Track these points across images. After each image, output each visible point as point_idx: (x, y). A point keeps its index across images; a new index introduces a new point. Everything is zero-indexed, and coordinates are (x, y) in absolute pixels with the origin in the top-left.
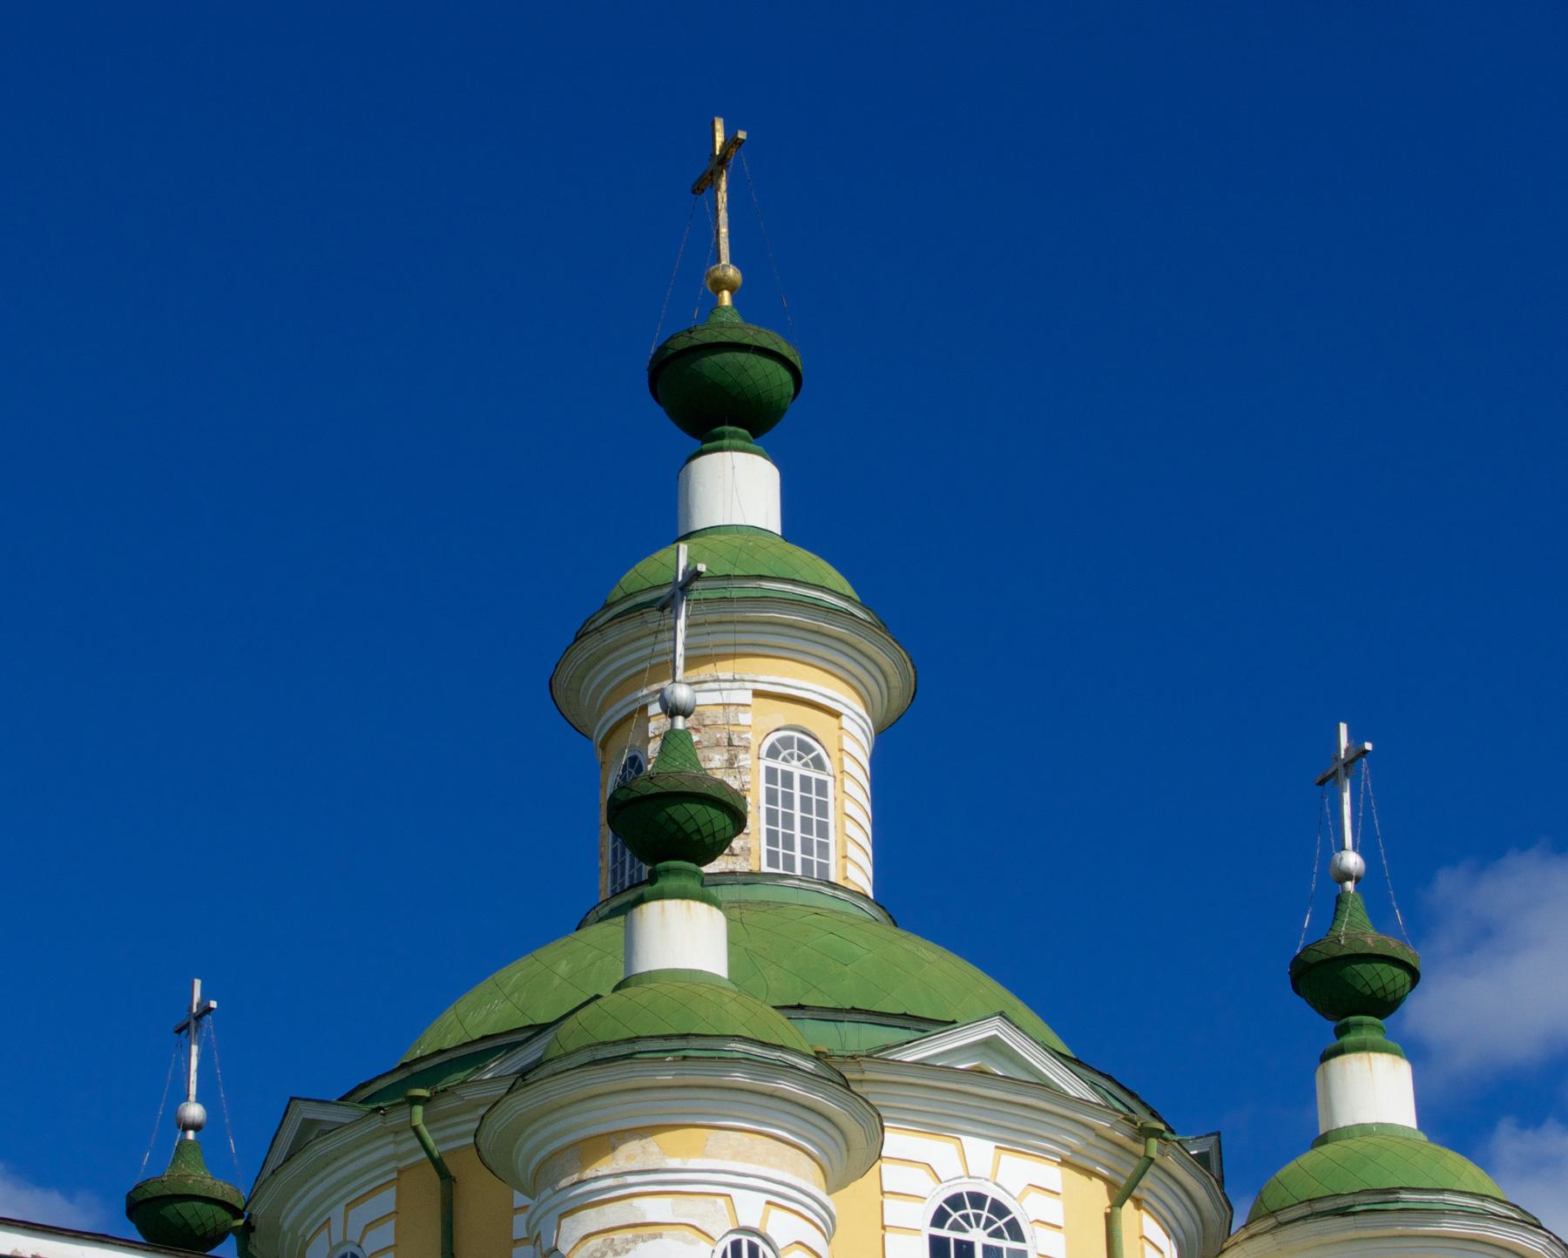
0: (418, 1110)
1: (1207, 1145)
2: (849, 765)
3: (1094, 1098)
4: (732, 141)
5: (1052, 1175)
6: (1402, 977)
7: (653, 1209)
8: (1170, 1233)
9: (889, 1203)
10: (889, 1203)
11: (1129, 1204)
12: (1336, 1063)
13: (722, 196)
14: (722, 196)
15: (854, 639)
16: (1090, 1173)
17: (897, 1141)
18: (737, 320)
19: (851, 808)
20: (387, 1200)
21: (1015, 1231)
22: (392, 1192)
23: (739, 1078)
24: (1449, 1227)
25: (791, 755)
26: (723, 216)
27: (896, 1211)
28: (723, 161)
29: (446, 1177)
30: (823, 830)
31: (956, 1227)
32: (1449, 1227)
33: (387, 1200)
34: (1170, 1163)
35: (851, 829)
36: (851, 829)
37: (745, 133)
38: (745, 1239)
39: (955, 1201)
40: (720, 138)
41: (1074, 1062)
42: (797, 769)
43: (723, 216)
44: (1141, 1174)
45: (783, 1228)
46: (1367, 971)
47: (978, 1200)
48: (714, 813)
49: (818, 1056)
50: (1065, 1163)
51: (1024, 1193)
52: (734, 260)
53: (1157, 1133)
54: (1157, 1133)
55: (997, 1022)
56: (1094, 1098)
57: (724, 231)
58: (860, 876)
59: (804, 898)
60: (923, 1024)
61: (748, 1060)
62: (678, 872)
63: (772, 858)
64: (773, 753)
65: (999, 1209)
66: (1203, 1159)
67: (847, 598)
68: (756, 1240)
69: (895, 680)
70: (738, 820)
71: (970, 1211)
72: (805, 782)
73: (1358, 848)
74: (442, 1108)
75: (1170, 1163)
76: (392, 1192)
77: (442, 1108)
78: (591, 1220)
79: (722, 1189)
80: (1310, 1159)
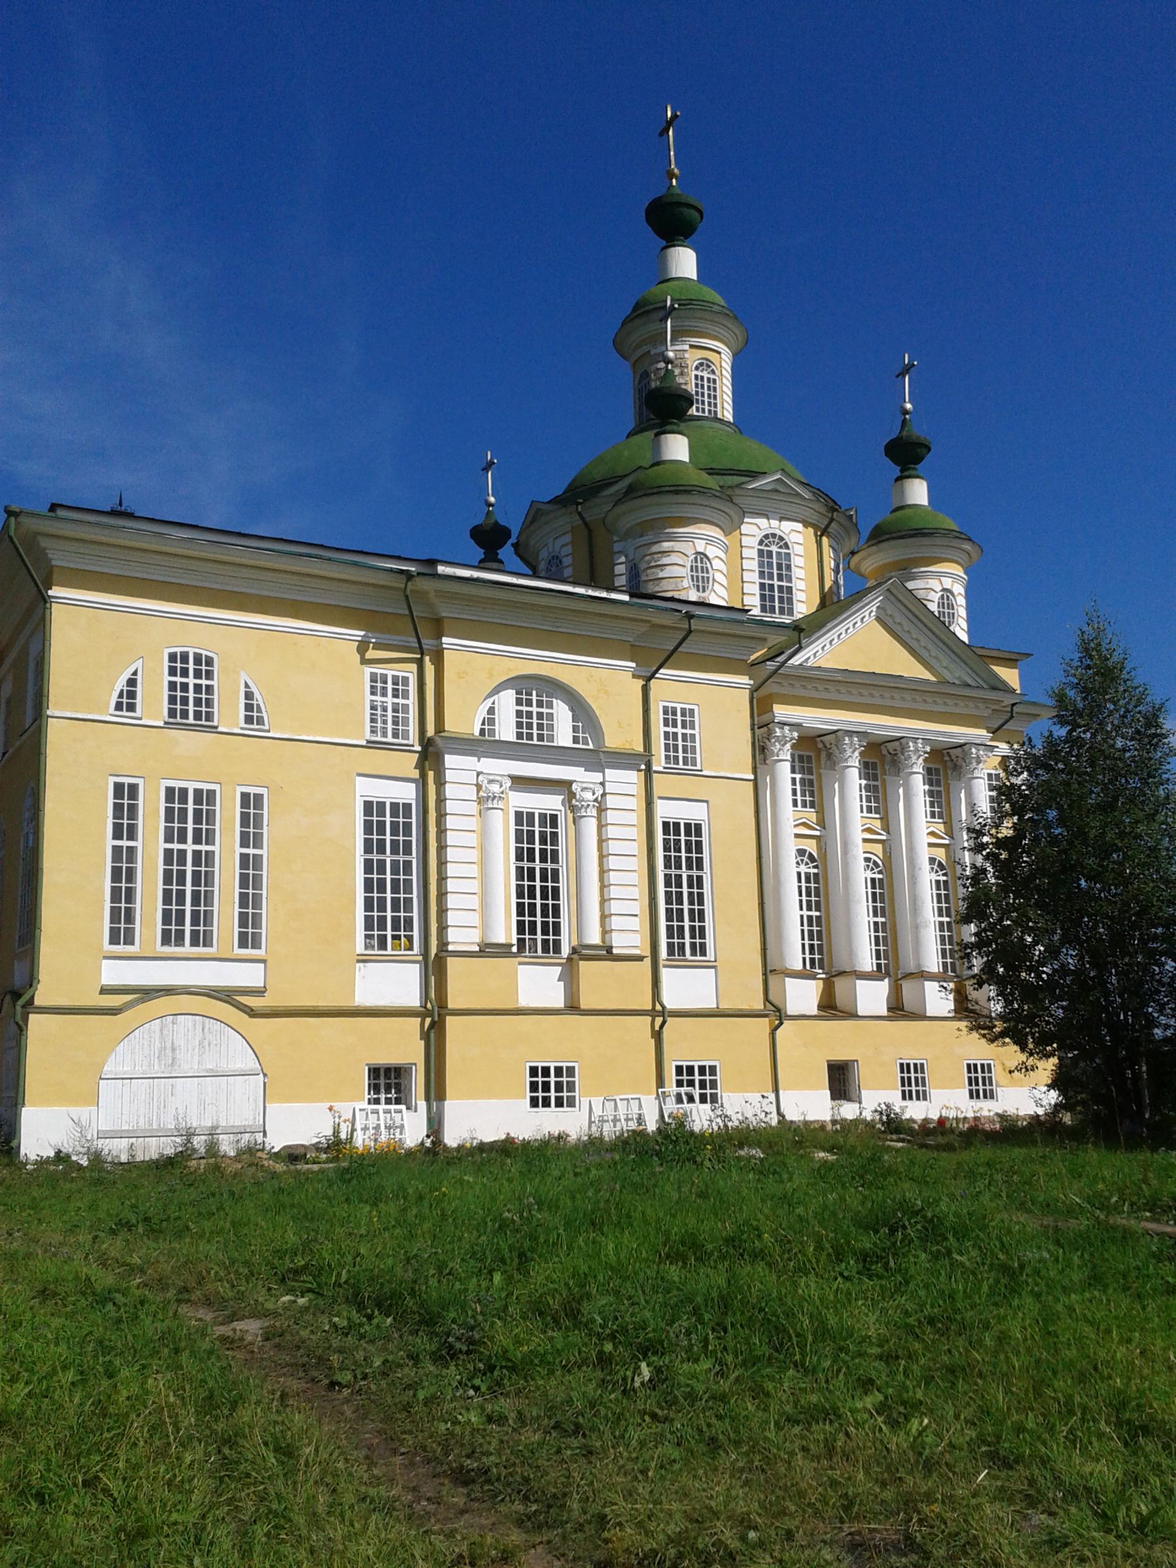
4: (674, 116)
5: (799, 526)
12: (663, 436)
20: (568, 538)
21: (786, 546)
27: (746, 541)
28: (669, 123)
29: (590, 531)
31: (766, 545)
39: (766, 536)
42: (706, 375)
45: (712, 551)
47: (774, 535)
60: (754, 475)
64: (697, 368)
65: (781, 539)
69: (740, 338)
72: (709, 379)
73: (910, 401)
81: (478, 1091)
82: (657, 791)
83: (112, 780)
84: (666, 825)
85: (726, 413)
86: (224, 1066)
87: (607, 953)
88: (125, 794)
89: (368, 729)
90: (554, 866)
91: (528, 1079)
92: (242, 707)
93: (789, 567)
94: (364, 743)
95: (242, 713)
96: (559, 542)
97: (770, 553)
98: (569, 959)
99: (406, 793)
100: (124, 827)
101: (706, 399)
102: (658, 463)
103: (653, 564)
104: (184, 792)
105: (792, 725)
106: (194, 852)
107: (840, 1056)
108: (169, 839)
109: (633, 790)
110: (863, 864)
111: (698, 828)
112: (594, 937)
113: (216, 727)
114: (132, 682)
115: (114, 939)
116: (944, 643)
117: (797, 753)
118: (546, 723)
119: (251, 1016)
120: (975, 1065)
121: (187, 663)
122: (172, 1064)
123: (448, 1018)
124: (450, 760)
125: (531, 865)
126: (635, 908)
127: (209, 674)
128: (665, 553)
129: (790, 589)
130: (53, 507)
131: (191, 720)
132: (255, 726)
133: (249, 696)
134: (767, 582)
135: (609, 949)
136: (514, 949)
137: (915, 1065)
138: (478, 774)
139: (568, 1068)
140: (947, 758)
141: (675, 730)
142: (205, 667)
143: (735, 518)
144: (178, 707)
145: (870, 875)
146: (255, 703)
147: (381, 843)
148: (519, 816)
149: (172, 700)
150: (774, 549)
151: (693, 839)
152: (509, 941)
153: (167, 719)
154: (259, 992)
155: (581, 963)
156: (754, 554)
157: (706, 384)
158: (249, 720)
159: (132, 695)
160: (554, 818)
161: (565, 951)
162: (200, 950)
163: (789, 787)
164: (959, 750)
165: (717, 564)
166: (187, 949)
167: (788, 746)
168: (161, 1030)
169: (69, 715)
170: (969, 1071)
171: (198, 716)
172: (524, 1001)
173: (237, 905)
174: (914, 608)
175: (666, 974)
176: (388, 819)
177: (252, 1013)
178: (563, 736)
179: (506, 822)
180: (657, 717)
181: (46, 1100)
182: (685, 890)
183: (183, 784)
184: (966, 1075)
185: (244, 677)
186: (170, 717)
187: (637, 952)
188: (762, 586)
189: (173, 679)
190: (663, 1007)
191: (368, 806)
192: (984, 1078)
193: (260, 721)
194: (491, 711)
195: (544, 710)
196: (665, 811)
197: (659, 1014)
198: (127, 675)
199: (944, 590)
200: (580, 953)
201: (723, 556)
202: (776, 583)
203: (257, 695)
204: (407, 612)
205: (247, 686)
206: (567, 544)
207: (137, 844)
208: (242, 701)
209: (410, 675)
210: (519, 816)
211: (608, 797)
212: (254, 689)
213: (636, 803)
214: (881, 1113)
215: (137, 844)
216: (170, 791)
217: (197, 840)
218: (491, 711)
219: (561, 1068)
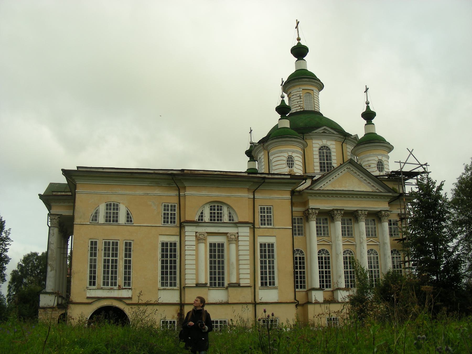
5: (334, 143)
21: (329, 149)
25: (322, 254)
31: (322, 150)
39: (322, 147)
47: (325, 146)
51: (330, 145)
65: (327, 147)
68: (291, 156)
71: (324, 148)
74: (390, 194)
77: (390, 194)
84: (261, 245)
88: (94, 244)
99: (175, 239)
108: (105, 256)
116: (137, 181)
118: (220, 216)
138: (196, 233)
147: (265, 256)
148: (211, 245)
154: (130, 298)
156: (317, 153)
171: (218, 220)
176: (217, 248)
178: (226, 218)
179: (206, 247)
180: (258, 209)
188: (320, 163)
191: (163, 244)
193: (131, 221)
196: (260, 240)
197: (255, 304)
200: (231, 285)
202: (326, 162)
209: (176, 204)
210: (211, 245)
211: (239, 237)
214: (117, 329)
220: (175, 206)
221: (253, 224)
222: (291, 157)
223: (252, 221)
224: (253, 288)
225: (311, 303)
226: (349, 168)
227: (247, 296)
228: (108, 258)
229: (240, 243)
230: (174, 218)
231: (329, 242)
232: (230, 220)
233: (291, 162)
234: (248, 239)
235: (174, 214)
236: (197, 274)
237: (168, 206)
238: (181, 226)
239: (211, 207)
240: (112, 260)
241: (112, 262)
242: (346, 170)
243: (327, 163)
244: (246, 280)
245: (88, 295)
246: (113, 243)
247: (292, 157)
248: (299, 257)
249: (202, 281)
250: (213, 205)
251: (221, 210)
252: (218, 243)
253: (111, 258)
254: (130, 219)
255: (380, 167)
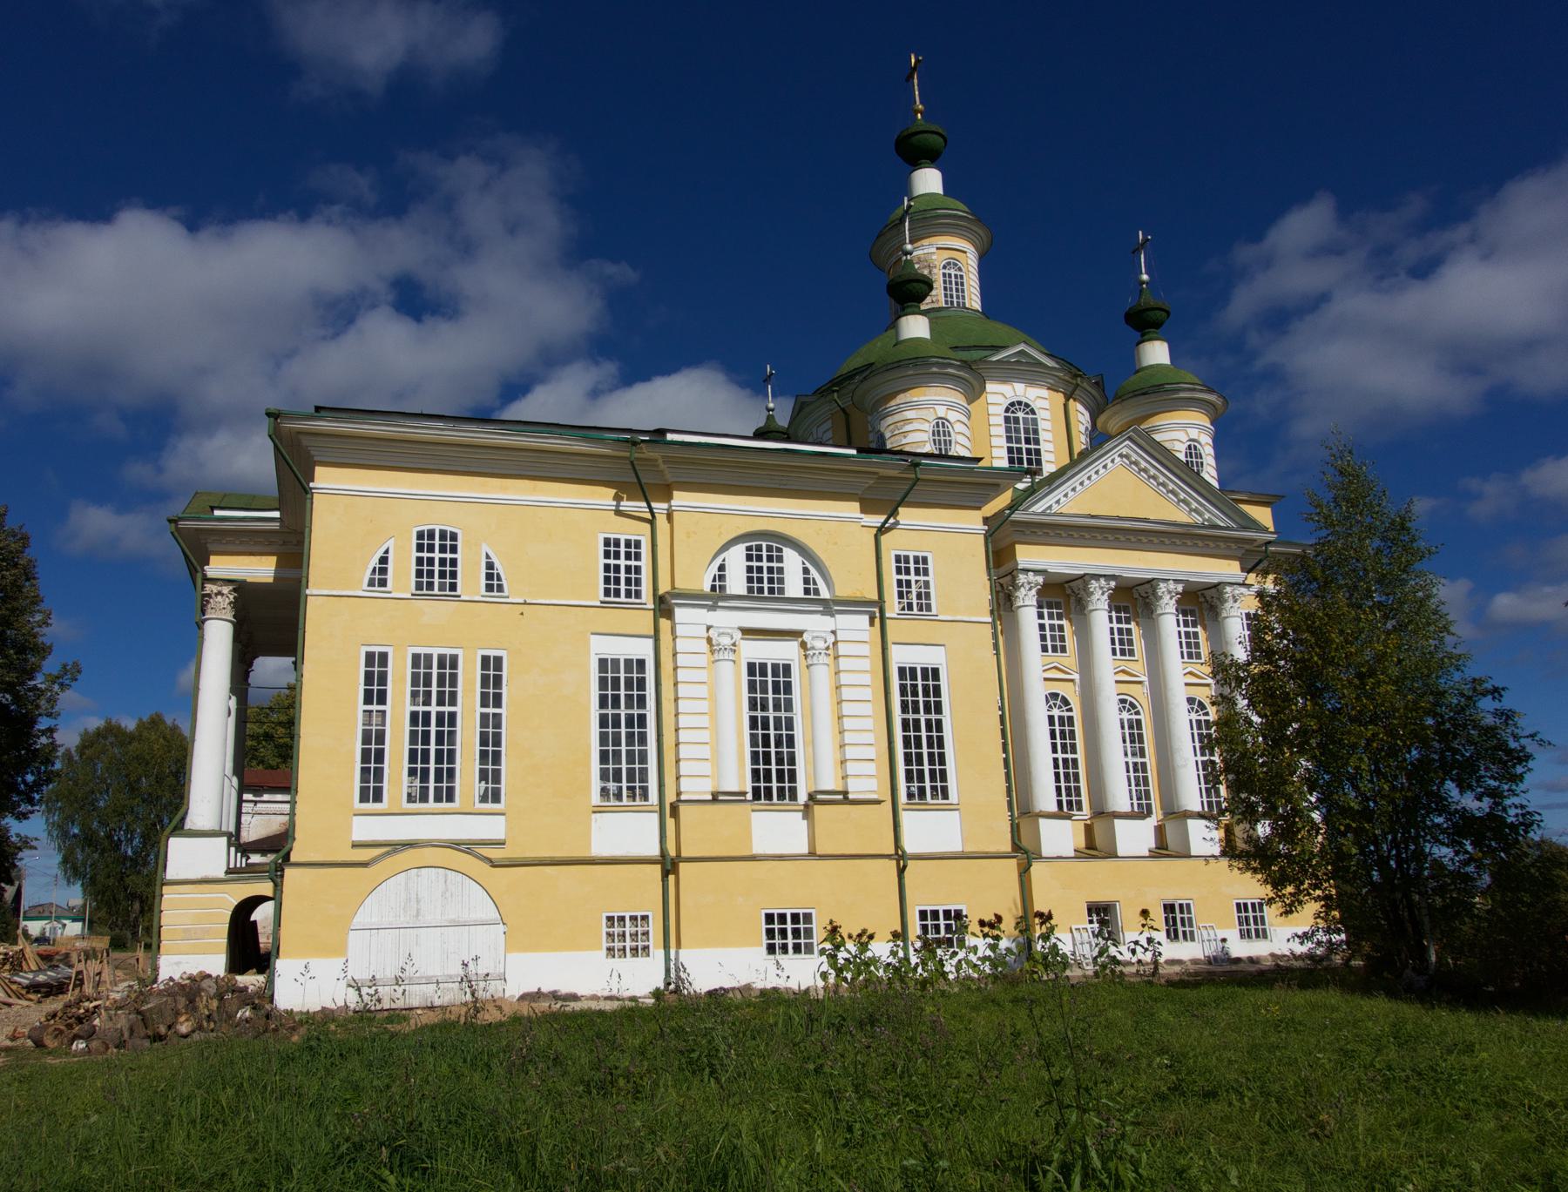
0: (836, 394)
1: (1098, 379)
2: (971, 269)
3: (1057, 366)
4: (917, 61)
5: (1044, 392)
6: (1164, 314)
7: (909, 415)
8: (1086, 408)
9: (990, 407)
10: (990, 407)
11: (1071, 400)
13: (916, 81)
14: (916, 81)
15: (969, 225)
16: (1058, 391)
17: (990, 387)
18: (923, 122)
19: (972, 283)
20: (828, 424)
21: (1033, 412)
22: (830, 421)
23: (934, 369)
24: (1182, 395)
26: (916, 87)
27: (992, 409)
28: (914, 69)
30: (963, 291)
31: (1013, 412)
32: (1182, 395)
33: (828, 424)
34: (1085, 385)
35: (972, 289)
36: (972, 289)
37: (1268, 830)
38: (940, 421)
39: (1012, 404)
40: (913, 61)
41: (1050, 356)
42: (953, 272)
43: (916, 87)
44: (1074, 390)
45: (953, 416)
46: (1151, 314)
47: (1020, 403)
48: (922, 285)
49: (961, 361)
50: (1049, 389)
52: (921, 103)
53: (1080, 376)
54: (1080, 376)
55: (1023, 344)
56: (1057, 366)
57: (917, 93)
58: (974, 301)
59: (960, 313)
60: (997, 348)
61: (937, 363)
62: (911, 306)
63: (946, 302)
64: (944, 267)
65: (1027, 405)
66: (1096, 383)
67: (967, 213)
69: (985, 239)
70: (931, 288)
72: (956, 276)
73: (1146, 273)
75: (1085, 385)
76: (830, 421)
78: (890, 420)
79: (933, 405)
80: (1134, 378)
81: (718, 938)
82: (890, 638)
83: (364, 650)
84: (902, 671)
85: (973, 303)
86: (466, 916)
87: (845, 798)
88: (376, 664)
89: (602, 592)
90: (906, 716)
91: (764, 927)
92: (483, 576)
93: (1036, 432)
94: (598, 604)
95: (483, 582)
96: (821, 429)
97: (1016, 420)
98: (806, 806)
99: (642, 649)
100: (375, 693)
101: (954, 293)
102: (898, 343)
103: (897, 432)
104: (429, 657)
105: (1037, 572)
106: (438, 713)
107: (1101, 897)
109: (865, 636)
110: (1186, 706)
111: (936, 672)
112: (829, 782)
113: (459, 596)
114: (384, 560)
115: (364, 798)
117: (1044, 600)
118: (776, 577)
119: (494, 866)
120: (1245, 905)
121: (434, 539)
122: (418, 914)
123: (681, 864)
124: (680, 614)
125: (916, 716)
126: (870, 753)
127: (454, 549)
128: (907, 421)
129: (1038, 452)
130: (318, 409)
131: (436, 591)
132: (495, 594)
133: (490, 566)
134: (1014, 445)
135: (845, 793)
136: (749, 797)
137: (1181, 905)
139: (805, 914)
140: (1202, 599)
141: (908, 577)
142: (449, 541)
143: (975, 383)
144: (425, 580)
145: (1194, 717)
146: (495, 572)
148: (751, 668)
149: (419, 574)
150: (1020, 415)
151: (931, 683)
152: (743, 790)
153: (414, 592)
155: (816, 807)
157: (953, 279)
158: (489, 588)
159: (383, 571)
160: (787, 668)
161: (802, 797)
162: (444, 805)
163: (1036, 633)
164: (1213, 590)
165: (959, 427)
166: (431, 804)
167: (1034, 592)
168: (407, 883)
169: (326, 592)
170: (1239, 911)
172: (758, 849)
173: (478, 761)
174: (1161, 454)
175: (907, 818)
177: (494, 864)
178: (794, 588)
180: (889, 566)
181: (289, 956)
182: (924, 734)
183: (428, 651)
184: (1236, 915)
185: (485, 548)
186: (417, 589)
187: (874, 796)
188: (1010, 450)
189: (420, 554)
190: (904, 852)
191: (603, 663)
192: (1255, 918)
193: (500, 588)
194: (722, 568)
195: (775, 565)
196: (901, 656)
197: (901, 858)
198: (380, 553)
199: (1191, 440)
201: (964, 419)
202: (1024, 446)
203: (497, 564)
204: (636, 481)
205: (488, 556)
206: (828, 430)
207: (457, 709)
208: (484, 571)
210: (751, 668)
212: (494, 559)
213: (870, 650)
215: (503, 711)
216: (416, 658)
217: (441, 702)
218: (722, 568)
219: (798, 914)
220: (638, 544)
221: (880, 603)
222: (943, 423)
223: (875, 597)
224: (888, 805)
225: (1040, 857)
226: (1127, 457)
227: (871, 830)
228: (426, 709)
229: (844, 664)
230: (638, 582)
231: (11, 994)
232: (807, 591)
233: (944, 436)
234: (865, 650)
235: (638, 570)
236: (716, 759)
237: (617, 543)
238: (664, 607)
239: (749, 549)
240: (440, 716)
241: (440, 722)
242: (1118, 460)
243: (1029, 451)
244: (867, 780)
245: (358, 836)
246: (442, 658)
247: (946, 423)
248: (1197, 721)
249: (732, 785)
250: (754, 544)
251: (780, 559)
252: (772, 664)
253: (434, 709)
254: (495, 582)
255: (1194, 460)
